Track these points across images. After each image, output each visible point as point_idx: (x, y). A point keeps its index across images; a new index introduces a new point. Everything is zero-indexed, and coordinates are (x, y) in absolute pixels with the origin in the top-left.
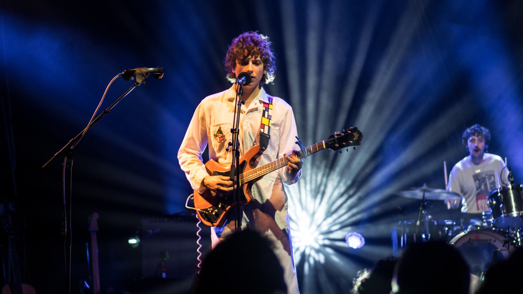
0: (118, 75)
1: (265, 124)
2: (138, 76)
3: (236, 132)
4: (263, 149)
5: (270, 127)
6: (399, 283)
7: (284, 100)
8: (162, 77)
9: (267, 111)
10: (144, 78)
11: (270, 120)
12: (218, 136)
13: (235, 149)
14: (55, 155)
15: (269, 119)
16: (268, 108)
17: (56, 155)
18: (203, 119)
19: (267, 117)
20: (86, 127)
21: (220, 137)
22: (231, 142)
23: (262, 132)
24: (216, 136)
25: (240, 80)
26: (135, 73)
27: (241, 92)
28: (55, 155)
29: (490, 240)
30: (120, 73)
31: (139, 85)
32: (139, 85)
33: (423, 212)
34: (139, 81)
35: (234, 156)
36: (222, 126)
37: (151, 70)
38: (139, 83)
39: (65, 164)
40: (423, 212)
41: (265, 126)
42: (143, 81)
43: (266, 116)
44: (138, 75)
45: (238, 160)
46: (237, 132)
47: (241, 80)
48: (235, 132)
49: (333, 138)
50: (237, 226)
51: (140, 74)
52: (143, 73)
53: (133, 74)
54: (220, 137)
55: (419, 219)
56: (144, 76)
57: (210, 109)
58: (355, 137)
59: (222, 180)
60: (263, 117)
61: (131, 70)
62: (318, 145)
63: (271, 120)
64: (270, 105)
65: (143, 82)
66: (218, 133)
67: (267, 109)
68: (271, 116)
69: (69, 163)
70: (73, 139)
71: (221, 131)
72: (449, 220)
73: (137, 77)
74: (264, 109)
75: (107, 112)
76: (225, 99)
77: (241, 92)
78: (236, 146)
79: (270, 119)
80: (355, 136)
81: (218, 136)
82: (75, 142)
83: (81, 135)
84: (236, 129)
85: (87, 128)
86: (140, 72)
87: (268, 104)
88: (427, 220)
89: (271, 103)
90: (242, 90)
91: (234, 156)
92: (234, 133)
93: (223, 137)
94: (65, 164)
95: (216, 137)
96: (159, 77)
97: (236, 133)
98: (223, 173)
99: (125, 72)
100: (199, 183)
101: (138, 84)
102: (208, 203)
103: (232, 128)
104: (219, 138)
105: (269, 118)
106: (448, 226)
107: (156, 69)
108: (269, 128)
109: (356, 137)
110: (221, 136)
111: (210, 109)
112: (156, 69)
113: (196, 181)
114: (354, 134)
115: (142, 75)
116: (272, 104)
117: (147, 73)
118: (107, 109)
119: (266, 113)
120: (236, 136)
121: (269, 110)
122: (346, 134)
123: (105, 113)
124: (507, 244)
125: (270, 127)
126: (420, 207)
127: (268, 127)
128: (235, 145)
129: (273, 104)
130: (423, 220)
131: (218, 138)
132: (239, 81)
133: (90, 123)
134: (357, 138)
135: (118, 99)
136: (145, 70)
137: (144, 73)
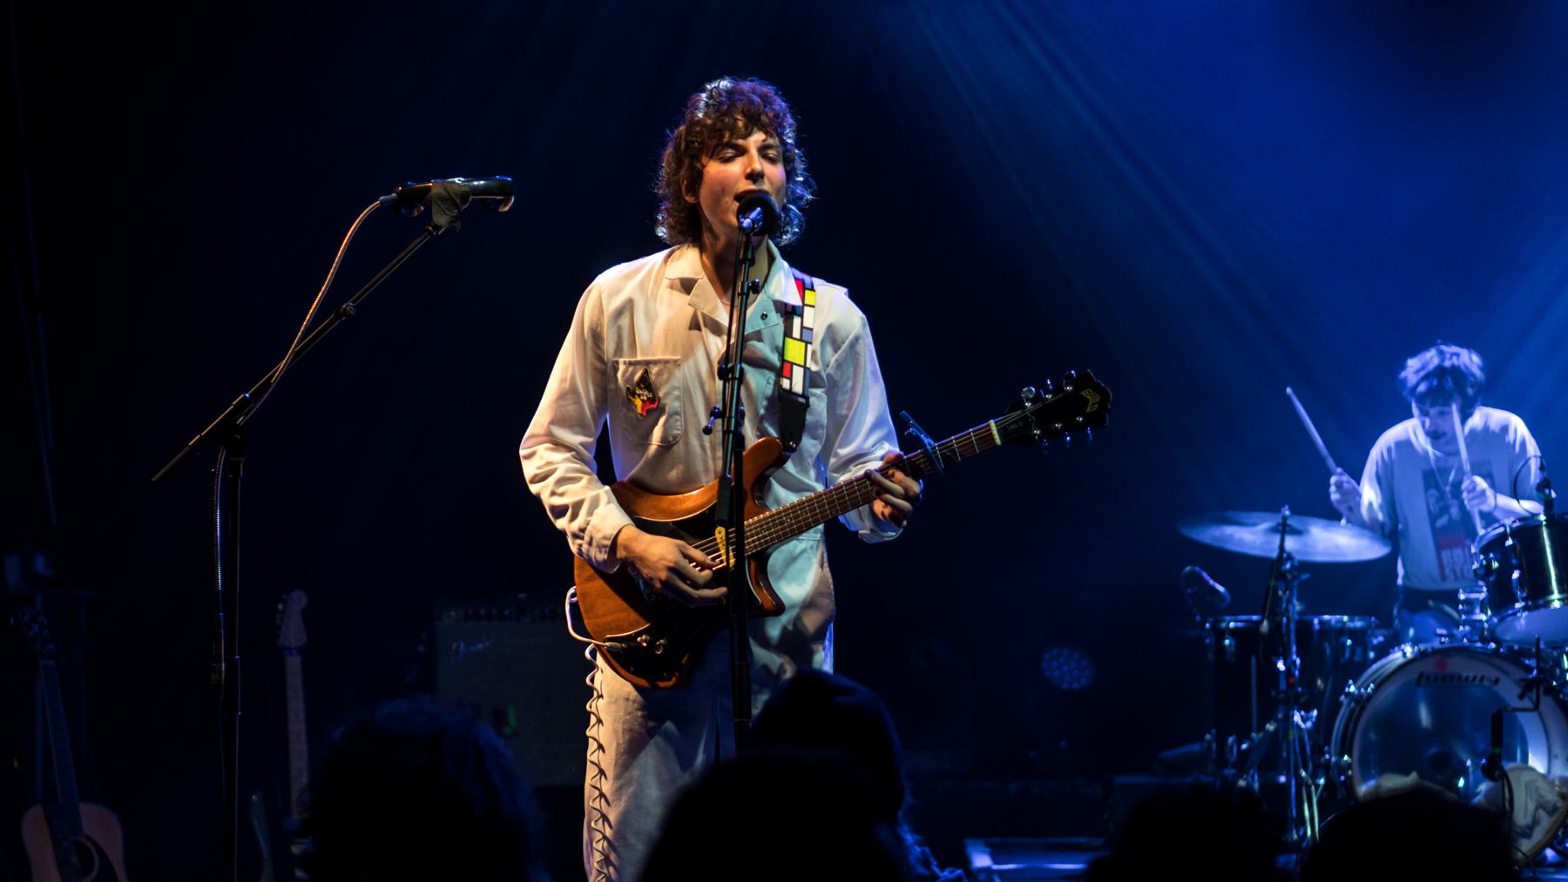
1: (794, 361)
3: (733, 375)
4: (791, 446)
6: (1185, 567)
7: (615, 265)
8: (507, 209)
9: (799, 316)
10: (456, 211)
11: (809, 346)
12: (639, 396)
13: (733, 428)
15: (807, 343)
18: (597, 337)
19: (798, 337)
21: (645, 398)
22: (720, 406)
23: (784, 390)
25: (745, 218)
26: (430, 194)
29: (1482, 679)
31: (440, 233)
32: (440, 233)
34: (441, 219)
36: (654, 370)
41: (794, 367)
43: (796, 333)
46: (737, 376)
47: (748, 220)
48: (730, 376)
49: (1020, 412)
51: (441, 199)
52: (453, 196)
56: (456, 206)
58: (1090, 403)
60: (788, 340)
62: (958, 448)
65: (451, 222)
66: (641, 389)
68: (812, 330)
69: (231, 467)
71: (650, 384)
72: (1357, 618)
76: (667, 280)
77: (750, 256)
78: (733, 419)
81: (639, 396)
83: (267, 383)
86: (445, 193)
93: (653, 403)
97: (733, 379)
99: (399, 194)
100: (605, 546)
101: (437, 228)
102: (633, 616)
104: (643, 401)
106: (1353, 633)
109: (1093, 404)
110: (649, 399)
113: (591, 539)
114: (1083, 393)
115: (450, 200)
117: (464, 196)
118: (344, 306)
120: (733, 389)
122: (1061, 395)
123: (338, 316)
124: (1535, 691)
127: (802, 370)
128: (730, 417)
132: (742, 223)
133: (295, 347)
134: (1096, 406)
135: (374, 280)
136: (1458, 355)
137: (456, 194)
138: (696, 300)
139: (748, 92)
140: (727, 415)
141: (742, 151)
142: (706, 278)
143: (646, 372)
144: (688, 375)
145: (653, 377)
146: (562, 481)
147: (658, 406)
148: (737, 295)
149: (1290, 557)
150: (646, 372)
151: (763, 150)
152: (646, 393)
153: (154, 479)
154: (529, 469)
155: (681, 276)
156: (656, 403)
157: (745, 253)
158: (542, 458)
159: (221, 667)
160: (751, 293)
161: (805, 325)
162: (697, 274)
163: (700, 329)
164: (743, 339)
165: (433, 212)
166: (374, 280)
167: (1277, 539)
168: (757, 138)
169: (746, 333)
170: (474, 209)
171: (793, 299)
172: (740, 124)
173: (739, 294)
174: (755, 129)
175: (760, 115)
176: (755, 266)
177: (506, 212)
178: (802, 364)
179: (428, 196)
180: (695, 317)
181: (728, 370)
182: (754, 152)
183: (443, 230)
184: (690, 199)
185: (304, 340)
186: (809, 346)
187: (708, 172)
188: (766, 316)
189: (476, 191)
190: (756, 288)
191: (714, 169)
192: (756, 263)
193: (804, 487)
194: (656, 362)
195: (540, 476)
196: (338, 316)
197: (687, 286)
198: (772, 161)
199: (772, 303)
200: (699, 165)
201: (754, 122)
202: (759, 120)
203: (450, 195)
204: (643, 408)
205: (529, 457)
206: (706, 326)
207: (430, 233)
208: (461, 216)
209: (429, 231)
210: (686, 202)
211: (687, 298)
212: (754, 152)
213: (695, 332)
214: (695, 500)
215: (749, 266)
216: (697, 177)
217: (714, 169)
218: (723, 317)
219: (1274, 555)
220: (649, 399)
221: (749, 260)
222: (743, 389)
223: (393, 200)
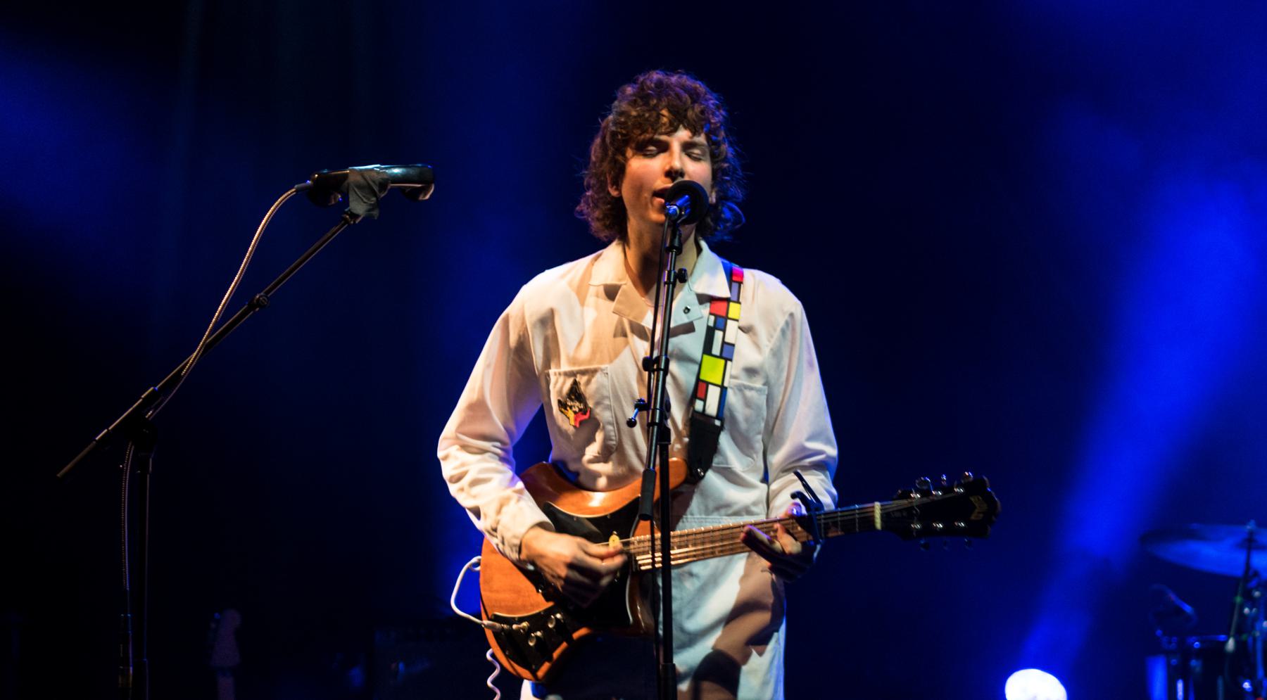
0: (293, 190)
2: (355, 191)
5: (726, 388)
8: (428, 197)
11: (729, 363)
12: (571, 407)
13: (657, 421)
14: (97, 438)
16: (726, 318)
17: (99, 439)
20: (194, 352)
21: (577, 410)
24: (563, 405)
26: (346, 182)
27: (676, 244)
28: (97, 438)
30: (297, 184)
31: (357, 222)
33: (1246, 610)
34: (359, 207)
35: (654, 442)
36: (582, 380)
37: (396, 174)
38: (357, 216)
39: (126, 466)
40: (1246, 610)
42: (369, 207)
43: (716, 349)
44: (356, 190)
45: (664, 456)
46: (662, 367)
48: (655, 367)
50: (764, 548)
51: (360, 187)
53: (339, 184)
54: (577, 410)
55: (1232, 632)
56: (375, 194)
57: (547, 321)
58: (977, 511)
59: (587, 553)
60: (706, 357)
61: (336, 175)
63: (731, 360)
64: (732, 305)
65: (369, 210)
66: (572, 400)
67: (721, 322)
70: (152, 389)
73: (352, 198)
74: (711, 324)
75: (259, 303)
77: (676, 244)
79: (728, 359)
80: (975, 508)
81: (571, 407)
82: (160, 399)
84: (658, 360)
85: (195, 354)
86: (362, 181)
87: (728, 300)
88: (1258, 634)
89: (735, 299)
90: (677, 237)
91: (654, 442)
92: (653, 372)
94: (126, 466)
95: (566, 409)
96: (419, 197)
97: (659, 369)
98: (605, 517)
99: (315, 181)
101: (355, 216)
103: (648, 355)
104: (575, 413)
105: (727, 353)
107: (411, 171)
108: (723, 390)
109: (979, 513)
110: (580, 410)
111: (547, 321)
112: (411, 171)
115: (367, 187)
116: (738, 302)
117: (383, 184)
118: (257, 297)
119: (718, 335)
120: (658, 381)
121: (729, 322)
123: (251, 307)
125: (726, 388)
126: (1236, 595)
127: (718, 390)
128: (655, 409)
129: (741, 300)
130: (1244, 637)
131: (571, 414)
133: (206, 339)
134: (981, 515)
135: (287, 271)
137: (374, 182)
138: (621, 307)
139: (675, 86)
140: (652, 407)
141: (664, 148)
142: (630, 283)
143: (575, 383)
144: (616, 384)
145: (582, 388)
146: (475, 483)
147: (590, 417)
148: (662, 284)
149: (1256, 574)
150: (575, 383)
151: (687, 147)
152: (577, 404)
153: (58, 475)
154: (447, 471)
155: (604, 283)
156: (588, 414)
157: (672, 241)
158: (456, 458)
159: (128, 670)
160: (678, 283)
161: (702, 377)
162: (620, 280)
163: (625, 335)
164: (669, 333)
165: (351, 199)
166: (287, 271)
167: (1241, 557)
168: (683, 134)
169: (672, 325)
170: (389, 195)
171: (720, 287)
172: (665, 120)
173: (665, 283)
174: (681, 126)
175: (686, 110)
176: (681, 255)
177: (427, 200)
178: (720, 383)
179: (346, 183)
180: (620, 323)
181: (653, 366)
182: (676, 147)
183: (360, 219)
184: (614, 193)
185: (213, 334)
186: (729, 363)
187: (630, 165)
188: (689, 310)
189: (396, 179)
190: (682, 277)
191: (637, 164)
192: (683, 252)
193: (776, 492)
194: (583, 373)
195: (456, 477)
196: (251, 307)
197: (611, 292)
198: (697, 159)
199: (695, 297)
200: (620, 158)
201: (679, 119)
202: (685, 117)
203: (369, 184)
204: (576, 420)
205: (446, 458)
206: (633, 331)
207: (347, 221)
208: (380, 204)
209: (346, 219)
210: (609, 193)
211: (612, 305)
212: (676, 147)
213: (620, 340)
214: (598, 502)
215: (676, 255)
216: (620, 171)
217: (637, 164)
218: (647, 322)
219: (1239, 572)
220: (580, 410)
221: (675, 248)
222: (669, 378)
223: (310, 188)
